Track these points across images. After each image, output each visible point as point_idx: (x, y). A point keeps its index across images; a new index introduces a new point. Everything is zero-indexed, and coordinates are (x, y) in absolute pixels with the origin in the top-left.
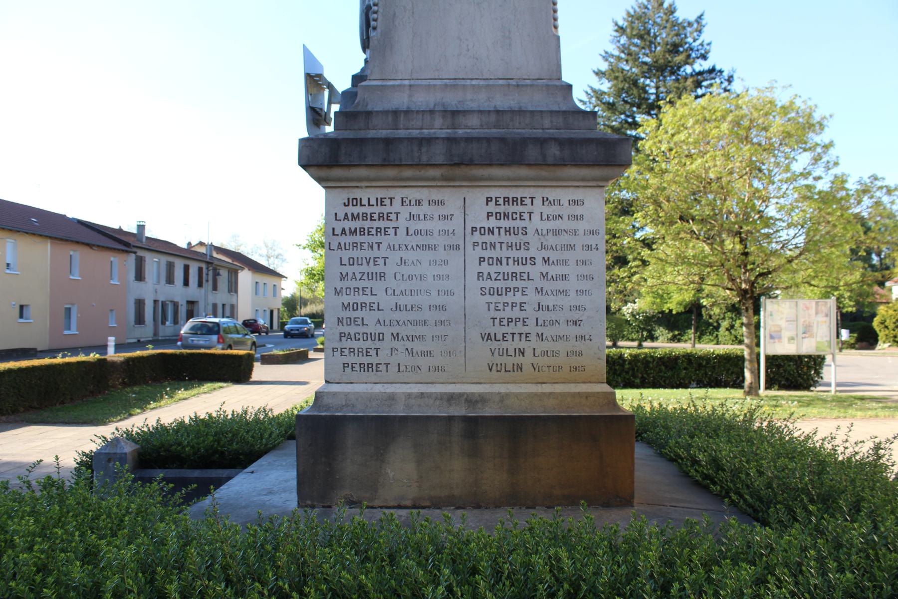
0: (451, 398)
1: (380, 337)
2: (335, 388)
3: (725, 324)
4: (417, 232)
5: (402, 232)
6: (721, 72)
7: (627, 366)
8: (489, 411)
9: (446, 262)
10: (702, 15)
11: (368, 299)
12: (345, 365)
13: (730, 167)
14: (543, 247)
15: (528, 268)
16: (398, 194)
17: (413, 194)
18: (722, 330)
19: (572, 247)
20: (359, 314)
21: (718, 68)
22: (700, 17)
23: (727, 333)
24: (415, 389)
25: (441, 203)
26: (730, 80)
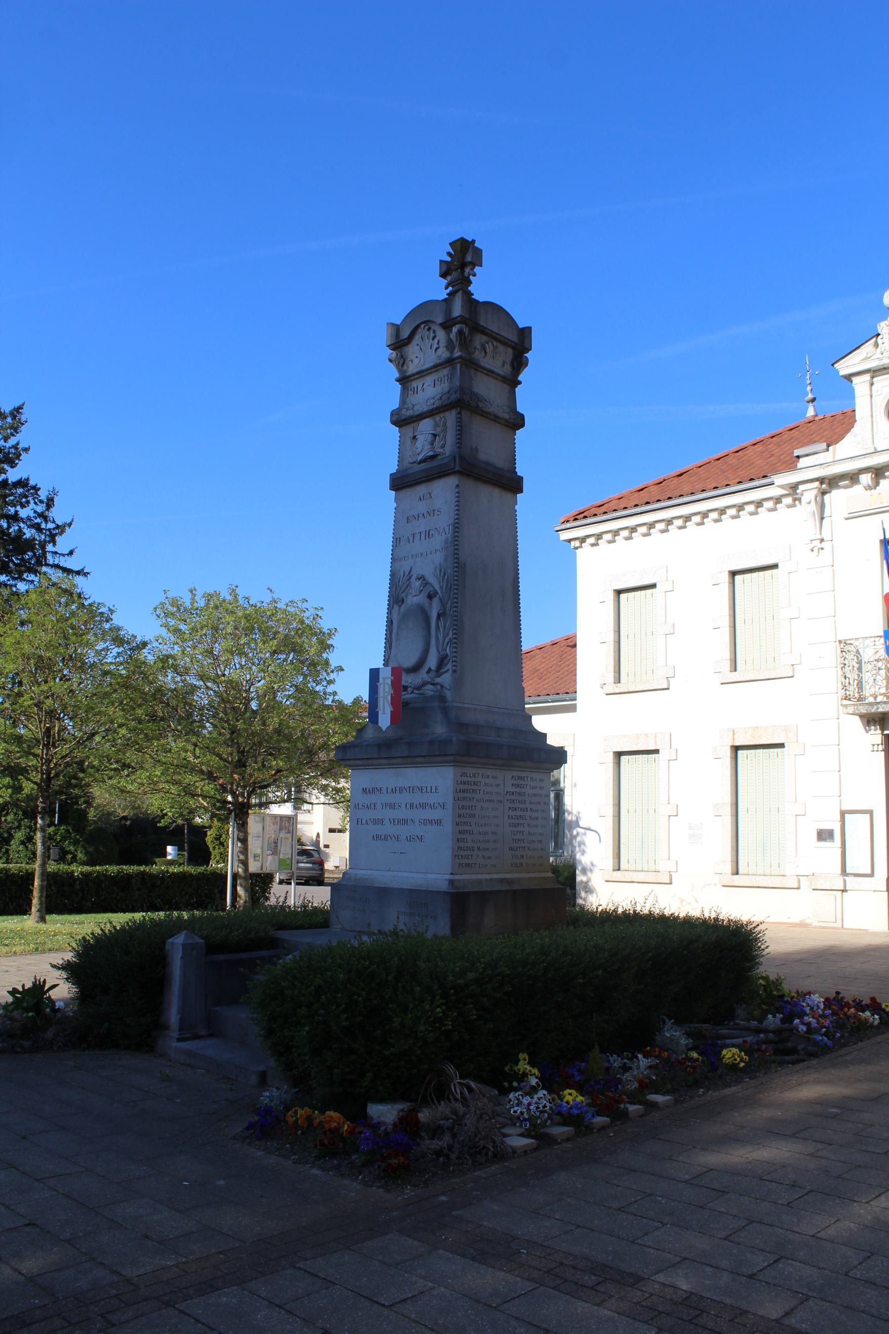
0: (502, 881)
1: (472, 849)
2: (457, 877)
3: (19, 835)
5: (482, 792)
6: (36, 489)
7: (77, 887)
8: (516, 887)
10: (20, 408)
11: (468, 828)
12: (460, 864)
16: (481, 771)
18: (14, 844)
20: (465, 836)
21: (32, 483)
22: (18, 410)
23: (21, 848)
24: (488, 876)
25: (496, 778)
26: (50, 503)
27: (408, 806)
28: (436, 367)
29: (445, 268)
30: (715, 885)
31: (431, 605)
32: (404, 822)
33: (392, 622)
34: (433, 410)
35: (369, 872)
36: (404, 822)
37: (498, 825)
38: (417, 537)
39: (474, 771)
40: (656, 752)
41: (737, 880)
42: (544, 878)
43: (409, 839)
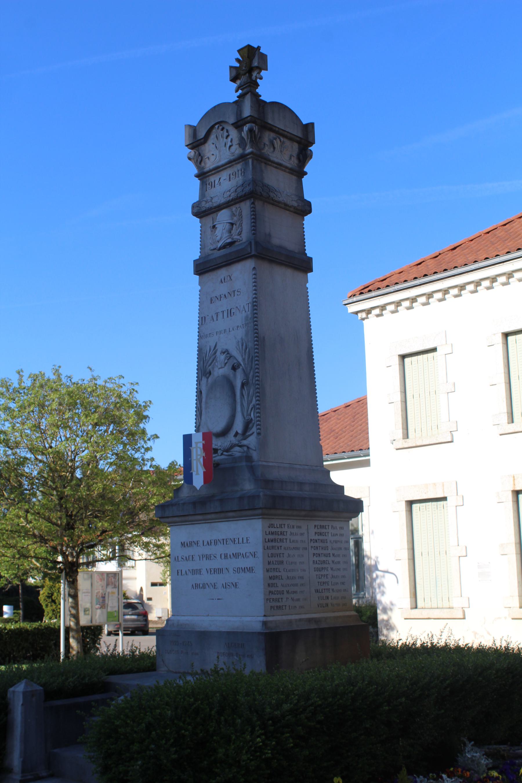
0: (310, 620)
1: (282, 593)
4: (293, 541)
8: (324, 625)
9: (303, 556)
12: (271, 607)
13: (28, 432)
14: (332, 549)
15: (328, 558)
16: (287, 522)
17: (292, 522)
19: (340, 549)
27: (223, 556)
28: (230, 163)
29: (234, 73)
30: (505, 618)
31: (235, 376)
32: (219, 571)
33: (201, 392)
34: (229, 202)
35: (190, 618)
36: (219, 571)
38: (220, 316)
40: (444, 499)
41: (415, 613)
43: (225, 586)
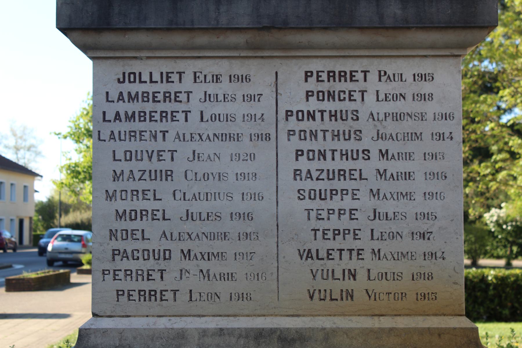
1: (167, 255)
5: (195, 116)
7: (491, 292)
11: (149, 205)
12: (119, 293)
16: (189, 67)
20: (137, 224)
24: (212, 323)
25: (245, 79)
37: (257, 197)
39: (166, 66)
42: (429, 331)
